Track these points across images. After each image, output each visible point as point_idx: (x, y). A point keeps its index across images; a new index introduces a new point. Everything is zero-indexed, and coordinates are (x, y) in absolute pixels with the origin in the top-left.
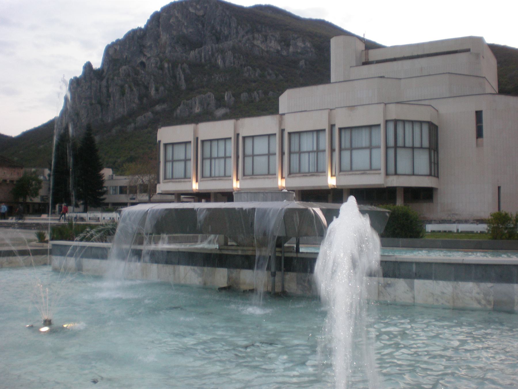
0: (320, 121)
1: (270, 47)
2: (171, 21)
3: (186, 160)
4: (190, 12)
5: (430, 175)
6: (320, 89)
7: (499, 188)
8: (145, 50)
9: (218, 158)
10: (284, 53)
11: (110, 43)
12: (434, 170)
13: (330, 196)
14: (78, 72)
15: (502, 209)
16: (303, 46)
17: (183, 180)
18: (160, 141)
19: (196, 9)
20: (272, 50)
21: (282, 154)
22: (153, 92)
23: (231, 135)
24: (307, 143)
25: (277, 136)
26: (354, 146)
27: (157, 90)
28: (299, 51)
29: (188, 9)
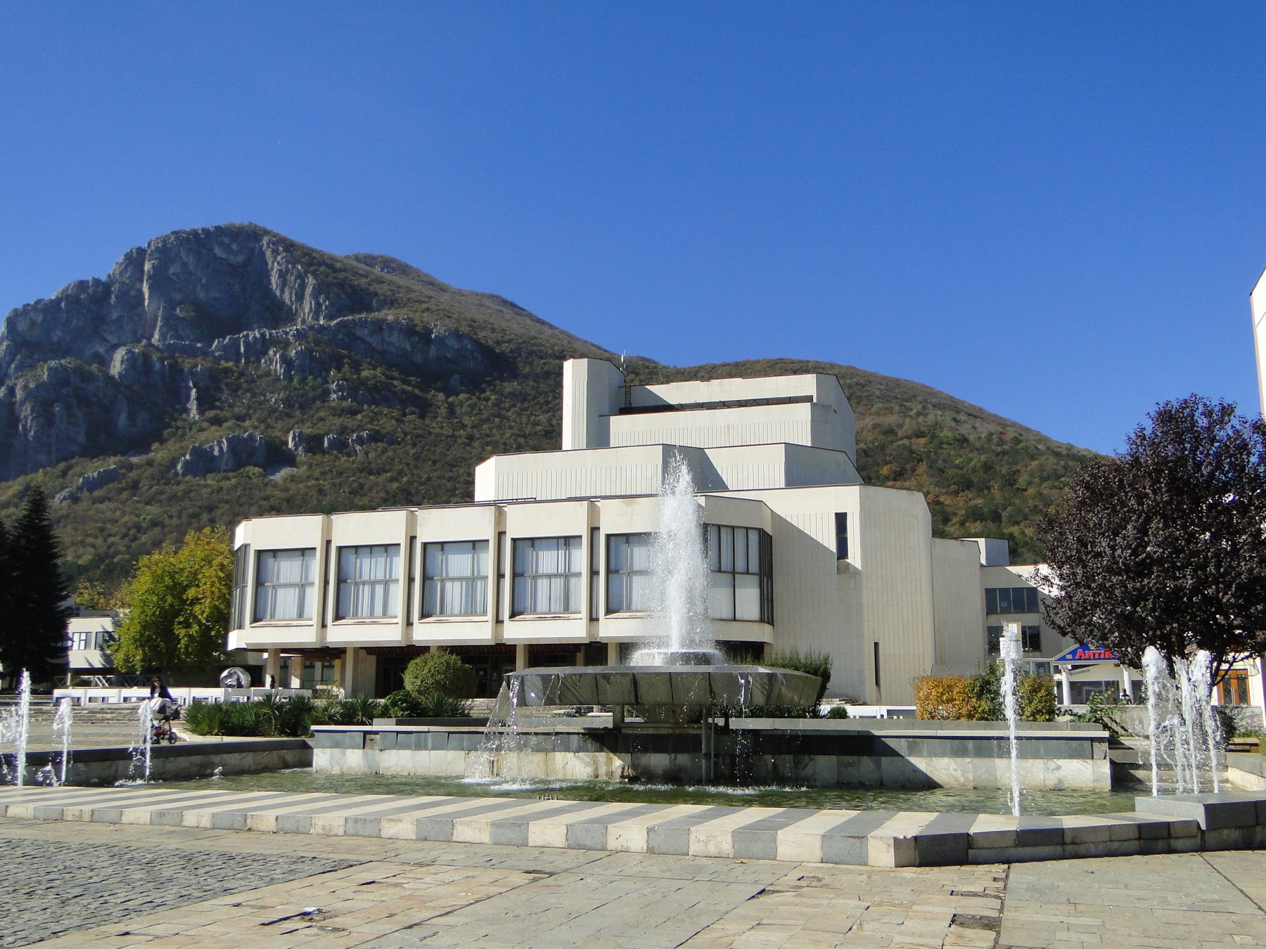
0: (573, 521)
1: (389, 344)
2: (171, 271)
4: (215, 257)
5: (762, 620)
6: (556, 455)
7: (876, 645)
8: (105, 327)
10: (418, 358)
11: (20, 306)
12: (767, 615)
13: (580, 656)
16: (457, 346)
17: (295, 623)
19: (227, 248)
20: (391, 348)
22: (123, 420)
23: (401, 539)
24: (548, 561)
25: (585, 541)
27: (132, 418)
28: (449, 355)
29: (211, 250)
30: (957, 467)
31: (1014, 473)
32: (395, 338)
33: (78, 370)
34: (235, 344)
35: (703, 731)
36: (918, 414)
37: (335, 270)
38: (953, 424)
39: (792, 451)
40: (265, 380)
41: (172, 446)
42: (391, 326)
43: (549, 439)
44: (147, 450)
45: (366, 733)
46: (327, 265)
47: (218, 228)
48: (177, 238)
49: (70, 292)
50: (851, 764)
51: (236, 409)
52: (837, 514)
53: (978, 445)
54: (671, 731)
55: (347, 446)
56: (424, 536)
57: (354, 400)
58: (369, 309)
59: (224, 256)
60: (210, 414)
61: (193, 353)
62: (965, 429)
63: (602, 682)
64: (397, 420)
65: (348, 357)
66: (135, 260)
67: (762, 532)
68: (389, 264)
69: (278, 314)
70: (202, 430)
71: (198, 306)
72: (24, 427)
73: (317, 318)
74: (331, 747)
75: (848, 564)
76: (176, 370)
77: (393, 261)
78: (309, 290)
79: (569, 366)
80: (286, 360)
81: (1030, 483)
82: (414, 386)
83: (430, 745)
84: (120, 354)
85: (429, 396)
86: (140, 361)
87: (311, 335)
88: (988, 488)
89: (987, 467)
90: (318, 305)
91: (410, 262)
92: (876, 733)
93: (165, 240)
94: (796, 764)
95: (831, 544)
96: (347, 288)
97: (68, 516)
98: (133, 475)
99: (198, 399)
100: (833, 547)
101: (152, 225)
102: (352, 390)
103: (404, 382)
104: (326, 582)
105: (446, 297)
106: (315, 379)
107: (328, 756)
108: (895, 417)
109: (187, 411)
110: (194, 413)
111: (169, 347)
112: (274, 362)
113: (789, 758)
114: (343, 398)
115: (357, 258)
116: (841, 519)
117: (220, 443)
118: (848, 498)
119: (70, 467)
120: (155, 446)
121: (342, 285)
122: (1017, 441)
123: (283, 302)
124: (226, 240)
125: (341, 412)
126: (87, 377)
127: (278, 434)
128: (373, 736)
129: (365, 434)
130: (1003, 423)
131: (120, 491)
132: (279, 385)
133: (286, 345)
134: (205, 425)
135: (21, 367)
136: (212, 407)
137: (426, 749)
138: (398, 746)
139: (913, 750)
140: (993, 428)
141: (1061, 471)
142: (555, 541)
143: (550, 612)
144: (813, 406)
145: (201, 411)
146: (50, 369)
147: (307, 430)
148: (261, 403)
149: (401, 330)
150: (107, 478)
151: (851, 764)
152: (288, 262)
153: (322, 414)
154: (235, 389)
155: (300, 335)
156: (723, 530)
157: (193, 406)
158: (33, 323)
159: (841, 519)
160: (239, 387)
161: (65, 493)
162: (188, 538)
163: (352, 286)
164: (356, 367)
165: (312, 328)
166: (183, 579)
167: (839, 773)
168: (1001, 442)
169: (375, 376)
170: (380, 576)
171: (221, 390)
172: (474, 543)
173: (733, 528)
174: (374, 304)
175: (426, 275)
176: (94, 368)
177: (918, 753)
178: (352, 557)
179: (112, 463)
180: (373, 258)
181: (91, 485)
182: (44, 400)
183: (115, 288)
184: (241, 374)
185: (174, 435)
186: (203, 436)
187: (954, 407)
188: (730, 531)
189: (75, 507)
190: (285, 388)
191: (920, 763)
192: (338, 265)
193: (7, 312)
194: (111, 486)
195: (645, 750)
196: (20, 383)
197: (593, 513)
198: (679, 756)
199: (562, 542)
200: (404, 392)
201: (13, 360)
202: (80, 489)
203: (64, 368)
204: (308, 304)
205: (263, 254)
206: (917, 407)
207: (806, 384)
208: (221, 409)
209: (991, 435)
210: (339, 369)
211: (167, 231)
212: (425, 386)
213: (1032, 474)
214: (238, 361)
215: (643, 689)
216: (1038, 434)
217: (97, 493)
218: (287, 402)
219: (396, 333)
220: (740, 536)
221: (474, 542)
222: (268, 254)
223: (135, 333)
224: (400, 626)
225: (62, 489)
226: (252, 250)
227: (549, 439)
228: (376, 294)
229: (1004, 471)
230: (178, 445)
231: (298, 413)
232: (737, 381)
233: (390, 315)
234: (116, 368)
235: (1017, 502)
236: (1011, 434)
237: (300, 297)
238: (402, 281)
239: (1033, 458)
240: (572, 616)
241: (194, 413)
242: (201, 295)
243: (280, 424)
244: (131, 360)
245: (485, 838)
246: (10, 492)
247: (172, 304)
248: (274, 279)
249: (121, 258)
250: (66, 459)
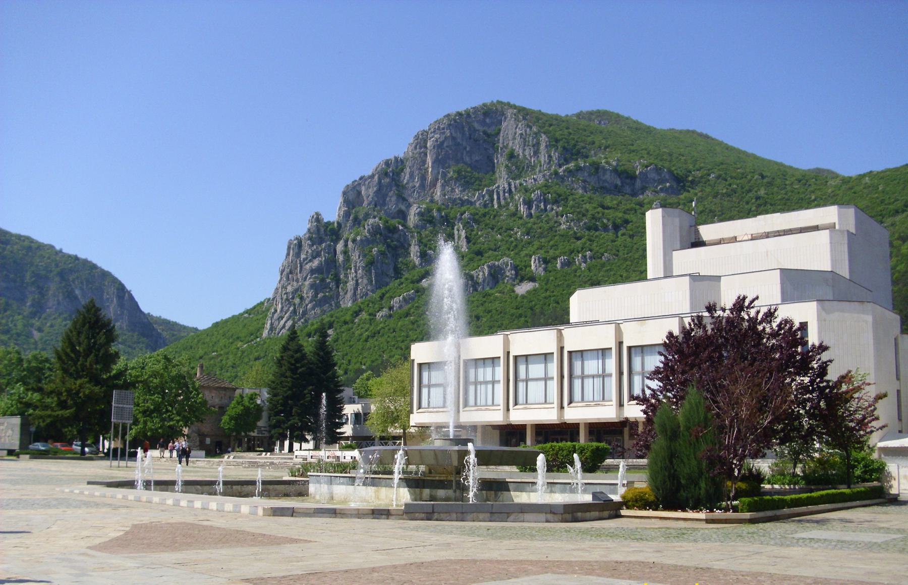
0: (605, 338)
1: (605, 181)
3: (604, 376)
9: (486, 383)
14: (302, 229)
21: (621, 373)
23: (500, 353)
25: (555, 355)
26: (586, 373)
43: (639, 274)
66: (421, 141)
68: (603, 115)
79: (649, 215)
90: (550, 157)
104: (562, 377)
142: (595, 352)
143: (593, 401)
170: (489, 378)
172: (546, 355)
183: (409, 164)
193: (342, 189)
197: (619, 332)
199: (600, 352)
204: (543, 158)
207: (829, 214)
211: (441, 116)
220: (483, 403)
224: (556, 409)
227: (639, 274)
237: (536, 153)
240: (607, 403)
245: (312, 488)
249: (411, 140)
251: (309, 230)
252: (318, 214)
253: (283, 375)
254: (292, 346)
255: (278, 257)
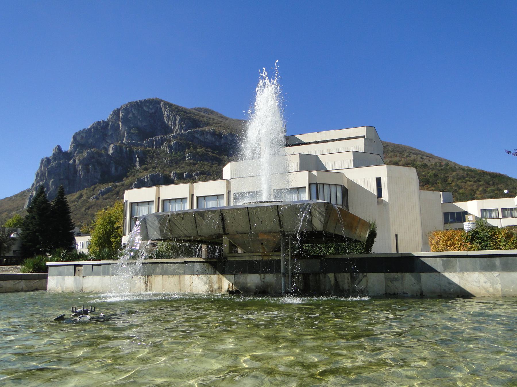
1: (207, 139)
2: (129, 116)
7: (396, 235)
10: (217, 144)
11: (78, 131)
14: (50, 153)
15: (400, 252)
18: (126, 201)
19: (149, 108)
20: (207, 141)
22: (113, 170)
27: (116, 169)
29: (143, 108)
30: (423, 175)
31: (446, 177)
32: (209, 137)
33: (97, 153)
34: (152, 141)
35: (282, 258)
36: (407, 156)
37: (187, 113)
38: (421, 160)
39: (356, 154)
40: (163, 154)
41: (130, 178)
42: (207, 133)
44: (122, 180)
45: (76, 266)
46: (183, 111)
47: (145, 100)
48: (131, 105)
49: (94, 125)
50: (396, 279)
51: (153, 165)
52: (376, 178)
53: (431, 167)
54: (261, 258)
55: (193, 176)
56: (197, 194)
57: (195, 160)
58: (199, 127)
59: (147, 110)
60: (144, 167)
61: (137, 145)
62: (426, 162)
63: (199, 218)
64: (210, 167)
65: (192, 144)
66: (116, 113)
67: (343, 187)
68: (206, 111)
69: (167, 130)
70: (141, 172)
71: (139, 129)
72: (79, 173)
73: (181, 130)
74: (57, 275)
75: (382, 200)
76: (131, 152)
77: (208, 109)
78: (177, 121)
80: (170, 146)
81: (453, 181)
82: (216, 154)
83: (111, 272)
84: (112, 146)
85: (222, 157)
86: (119, 149)
87: (179, 137)
88: (436, 183)
89: (436, 175)
90: (181, 126)
91: (214, 110)
92: (416, 254)
93: (126, 105)
94: (353, 278)
95: (375, 192)
96: (191, 119)
97: (95, 204)
98: (117, 189)
99: (139, 161)
100: (375, 192)
101: (121, 101)
102: (193, 156)
103: (213, 153)
105: (227, 121)
106: (180, 153)
107: (56, 281)
108: (398, 158)
109: (136, 166)
110: (138, 167)
111: (128, 143)
112: (166, 148)
113: (347, 275)
114: (190, 159)
115: (195, 109)
116: (379, 181)
117: (147, 177)
118: (381, 171)
119: (95, 187)
120: (125, 178)
121: (189, 118)
122: (447, 165)
123: (169, 126)
124: (148, 104)
125: (189, 164)
126: (100, 155)
127: (167, 173)
128: (80, 268)
129: (199, 172)
130: (441, 160)
131: (113, 195)
132: (168, 155)
133: (170, 141)
134: (142, 171)
135: (78, 153)
136: (144, 164)
137: (108, 275)
138: (92, 273)
139: (447, 267)
140: (437, 161)
141: (465, 176)
144: (365, 139)
145: (140, 166)
146: (87, 153)
147: (178, 171)
148: (161, 162)
149: (211, 134)
150: (108, 191)
151: (396, 279)
152: (170, 111)
153: (183, 165)
154: (152, 157)
155: (174, 137)
156: (325, 186)
157: (137, 164)
158: (82, 137)
159: (379, 181)
160: (153, 157)
161: (94, 196)
162: (116, 203)
163: (193, 119)
164: (195, 148)
165: (179, 134)
166: (113, 219)
167: (387, 286)
168: (440, 166)
169: (202, 151)
171: (147, 158)
173: (330, 185)
174: (201, 125)
175: (220, 114)
176: (103, 152)
177: (452, 269)
178: (168, 204)
179: (110, 185)
180: (201, 109)
181: (103, 193)
182: (86, 164)
183: (110, 123)
184: (154, 152)
185: (131, 174)
186: (141, 175)
187: (421, 154)
188: (328, 186)
189: (97, 201)
190: (170, 156)
191: (455, 277)
192: (188, 111)
194: (109, 193)
195: (244, 272)
196: (77, 158)
198: (267, 275)
200: (212, 156)
201: (76, 151)
202: (99, 195)
203: (92, 152)
205: (161, 109)
206: (406, 154)
208: (147, 165)
209: (436, 163)
210: (189, 149)
212: (220, 154)
213: (454, 177)
214: (153, 147)
215: (228, 220)
216: (455, 163)
217: (104, 196)
218: (171, 161)
219: (209, 135)
220: (333, 189)
221: (218, 195)
222: (163, 108)
223: (117, 139)
225: (93, 195)
226: (158, 107)
228: (202, 121)
229: (442, 177)
230: (132, 178)
231: (174, 165)
232: (333, 131)
233: (207, 129)
234: (110, 151)
235: (448, 188)
236: (444, 163)
237: (175, 124)
238: (211, 116)
239: (454, 171)
241: (138, 167)
242: (140, 124)
243: (168, 169)
244: (115, 149)
246: (75, 197)
247: (130, 128)
248: (165, 117)
249: (112, 113)
250: (94, 185)
251: (53, 154)
252: (59, 146)
253: (33, 218)
254: (41, 198)
255: (35, 167)
